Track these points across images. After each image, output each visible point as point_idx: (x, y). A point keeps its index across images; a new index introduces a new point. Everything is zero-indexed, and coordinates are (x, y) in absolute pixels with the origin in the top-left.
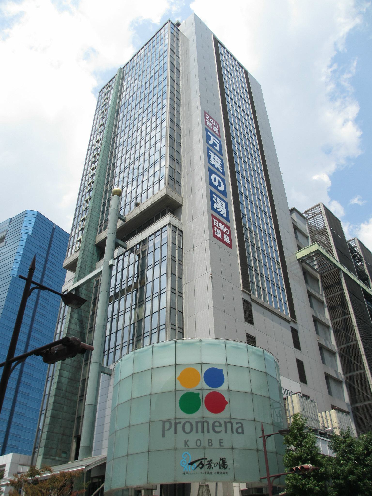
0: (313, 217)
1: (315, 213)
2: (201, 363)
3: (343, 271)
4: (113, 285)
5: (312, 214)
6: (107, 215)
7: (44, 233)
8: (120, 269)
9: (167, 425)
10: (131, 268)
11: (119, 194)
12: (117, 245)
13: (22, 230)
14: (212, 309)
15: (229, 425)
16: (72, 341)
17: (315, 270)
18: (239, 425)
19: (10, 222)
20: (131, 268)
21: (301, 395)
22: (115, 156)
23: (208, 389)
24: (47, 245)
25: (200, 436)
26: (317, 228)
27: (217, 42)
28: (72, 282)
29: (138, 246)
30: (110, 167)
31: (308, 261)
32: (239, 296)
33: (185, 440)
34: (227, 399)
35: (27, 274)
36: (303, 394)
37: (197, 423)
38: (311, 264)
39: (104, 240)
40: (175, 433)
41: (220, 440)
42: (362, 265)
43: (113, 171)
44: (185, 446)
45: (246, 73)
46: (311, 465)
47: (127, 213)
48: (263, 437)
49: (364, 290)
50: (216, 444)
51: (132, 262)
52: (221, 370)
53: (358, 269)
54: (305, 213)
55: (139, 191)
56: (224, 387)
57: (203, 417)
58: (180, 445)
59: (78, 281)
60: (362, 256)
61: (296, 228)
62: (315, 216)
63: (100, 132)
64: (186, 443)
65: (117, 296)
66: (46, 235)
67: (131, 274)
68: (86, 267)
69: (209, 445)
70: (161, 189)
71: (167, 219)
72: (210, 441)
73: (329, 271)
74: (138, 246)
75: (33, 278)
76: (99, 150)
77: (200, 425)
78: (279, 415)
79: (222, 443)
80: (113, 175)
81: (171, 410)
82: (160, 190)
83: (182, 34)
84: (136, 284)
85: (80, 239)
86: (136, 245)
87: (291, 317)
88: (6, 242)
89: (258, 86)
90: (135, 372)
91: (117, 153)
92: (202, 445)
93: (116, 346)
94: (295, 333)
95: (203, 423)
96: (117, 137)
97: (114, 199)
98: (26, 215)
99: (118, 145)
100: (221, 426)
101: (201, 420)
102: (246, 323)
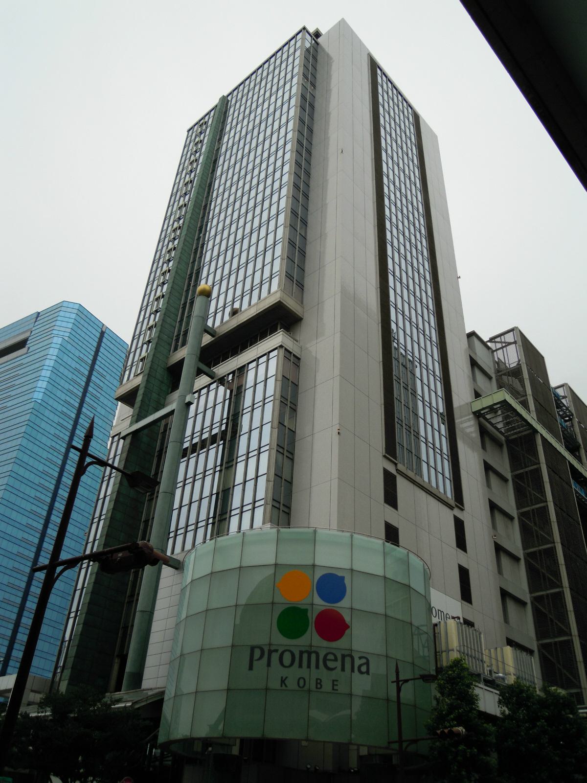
0: (502, 348)
1: (505, 343)
2: (314, 566)
3: (541, 435)
4: (188, 432)
5: (501, 342)
6: (188, 323)
7: (87, 338)
8: (201, 409)
9: (257, 653)
10: (219, 408)
11: (207, 294)
12: (199, 372)
13: (54, 332)
14: (335, 483)
15: (348, 660)
16: (141, 548)
17: (501, 432)
18: (364, 661)
19: (37, 318)
20: (219, 408)
21: (462, 621)
22: (205, 234)
23: (320, 605)
24: (91, 358)
25: (304, 672)
26: (507, 365)
27: (374, 66)
28: (128, 421)
29: (230, 377)
30: (196, 249)
31: (488, 417)
32: (378, 465)
33: (282, 677)
34: (347, 619)
35: (82, 442)
36: (464, 619)
37: (301, 653)
38: (493, 421)
39: (181, 362)
40: (269, 665)
41: (333, 681)
42: (572, 426)
43: (201, 257)
44: (281, 686)
45: (416, 117)
46: (464, 730)
47: (218, 323)
48: (397, 681)
49: (572, 466)
50: (327, 686)
51: (220, 399)
52: (343, 578)
53: (566, 432)
54: (492, 340)
55: (240, 285)
56: (345, 603)
57: (311, 646)
58: (275, 684)
59: (137, 421)
60: (573, 412)
61: (474, 363)
62: (506, 346)
63: (185, 194)
64: (283, 681)
65: (194, 448)
66: (91, 341)
67: (217, 418)
68: (150, 401)
69: (317, 688)
70: (272, 291)
71: (278, 338)
72: (319, 681)
73: (520, 432)
74: (230, 377)
75: (90, 448)
76: (181, 222)
77: (305, 656)
78: (426, 645)
79: (337, 685)
80: (200, 262)
81: (265, 632)
82: (272, 292)
83: (323, 50)
84: (224, 433)
85: (144, 358)
86: (229, 374)
87: (456, 500)
88: (29, 348)
89: (434, 137)
90: (214, 571)
91: (208, 229)
92: (306, 688)
93: (187, 526)
94: (459, 525)
95: (309, 654)
96: (211, 204)
97: (199, 302)
98: (63, 309)
99: (211, 216)
100: (336, 659)
101: (307, 649)
102: (386, 506)
